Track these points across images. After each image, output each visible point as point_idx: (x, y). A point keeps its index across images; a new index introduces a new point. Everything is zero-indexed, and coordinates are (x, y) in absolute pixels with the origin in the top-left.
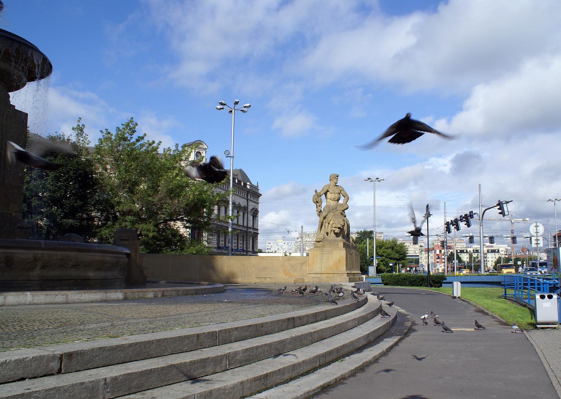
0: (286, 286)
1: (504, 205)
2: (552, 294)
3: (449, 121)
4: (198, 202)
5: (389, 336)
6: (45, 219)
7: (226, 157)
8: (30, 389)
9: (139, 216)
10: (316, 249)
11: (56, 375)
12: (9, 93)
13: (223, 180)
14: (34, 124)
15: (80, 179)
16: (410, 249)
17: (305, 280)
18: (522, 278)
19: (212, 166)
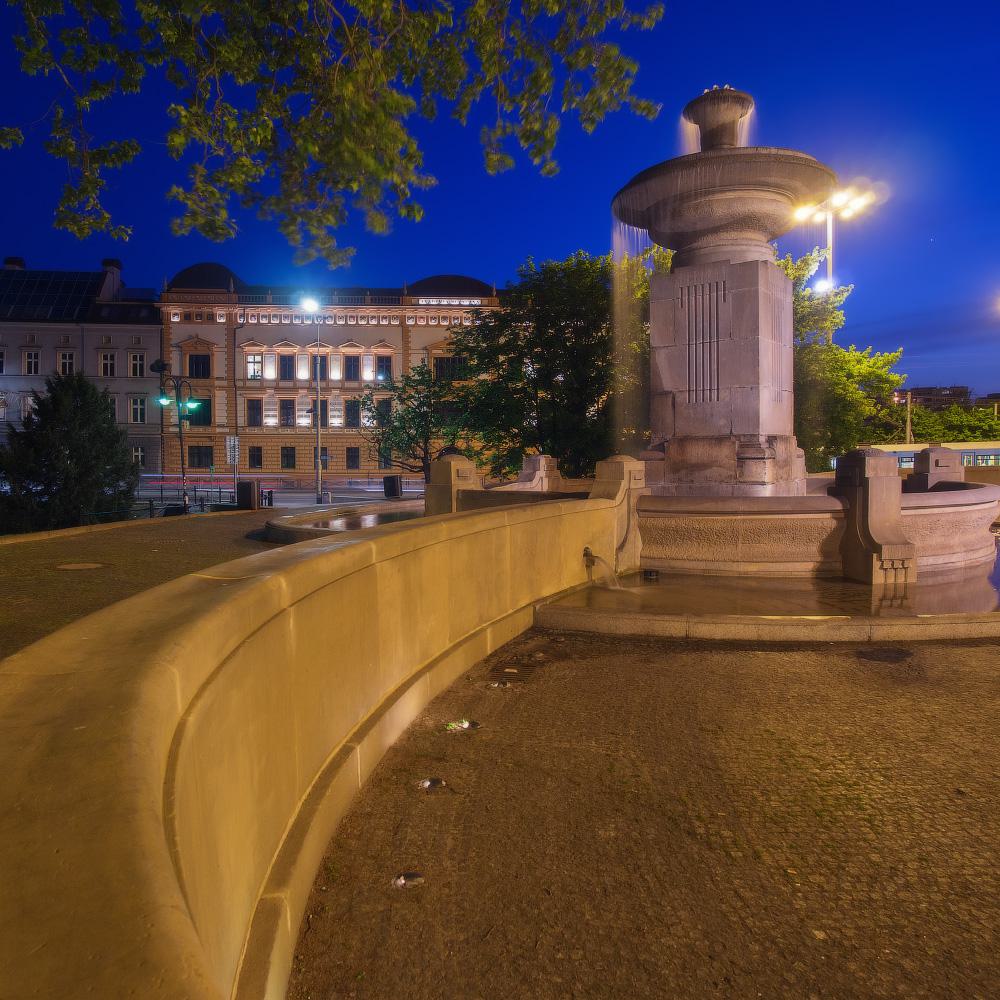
0: (684, 276)
1: (224, 375)
2: (762, 439)
3: (812, 216)
4: (518, 22)
5: (68, 620)
6: (317, 149)
7: (36, 372)
8: (725, 300)
9: (332, 153)
10: (386, 527)
11: (945, 388)
12: (683, 119)
13: (420, 147)
14: (483, 976)
15: (560, 378)
16: (726, 146)
17: (586, 580)
18: (232, 290)
19: (507, 670)
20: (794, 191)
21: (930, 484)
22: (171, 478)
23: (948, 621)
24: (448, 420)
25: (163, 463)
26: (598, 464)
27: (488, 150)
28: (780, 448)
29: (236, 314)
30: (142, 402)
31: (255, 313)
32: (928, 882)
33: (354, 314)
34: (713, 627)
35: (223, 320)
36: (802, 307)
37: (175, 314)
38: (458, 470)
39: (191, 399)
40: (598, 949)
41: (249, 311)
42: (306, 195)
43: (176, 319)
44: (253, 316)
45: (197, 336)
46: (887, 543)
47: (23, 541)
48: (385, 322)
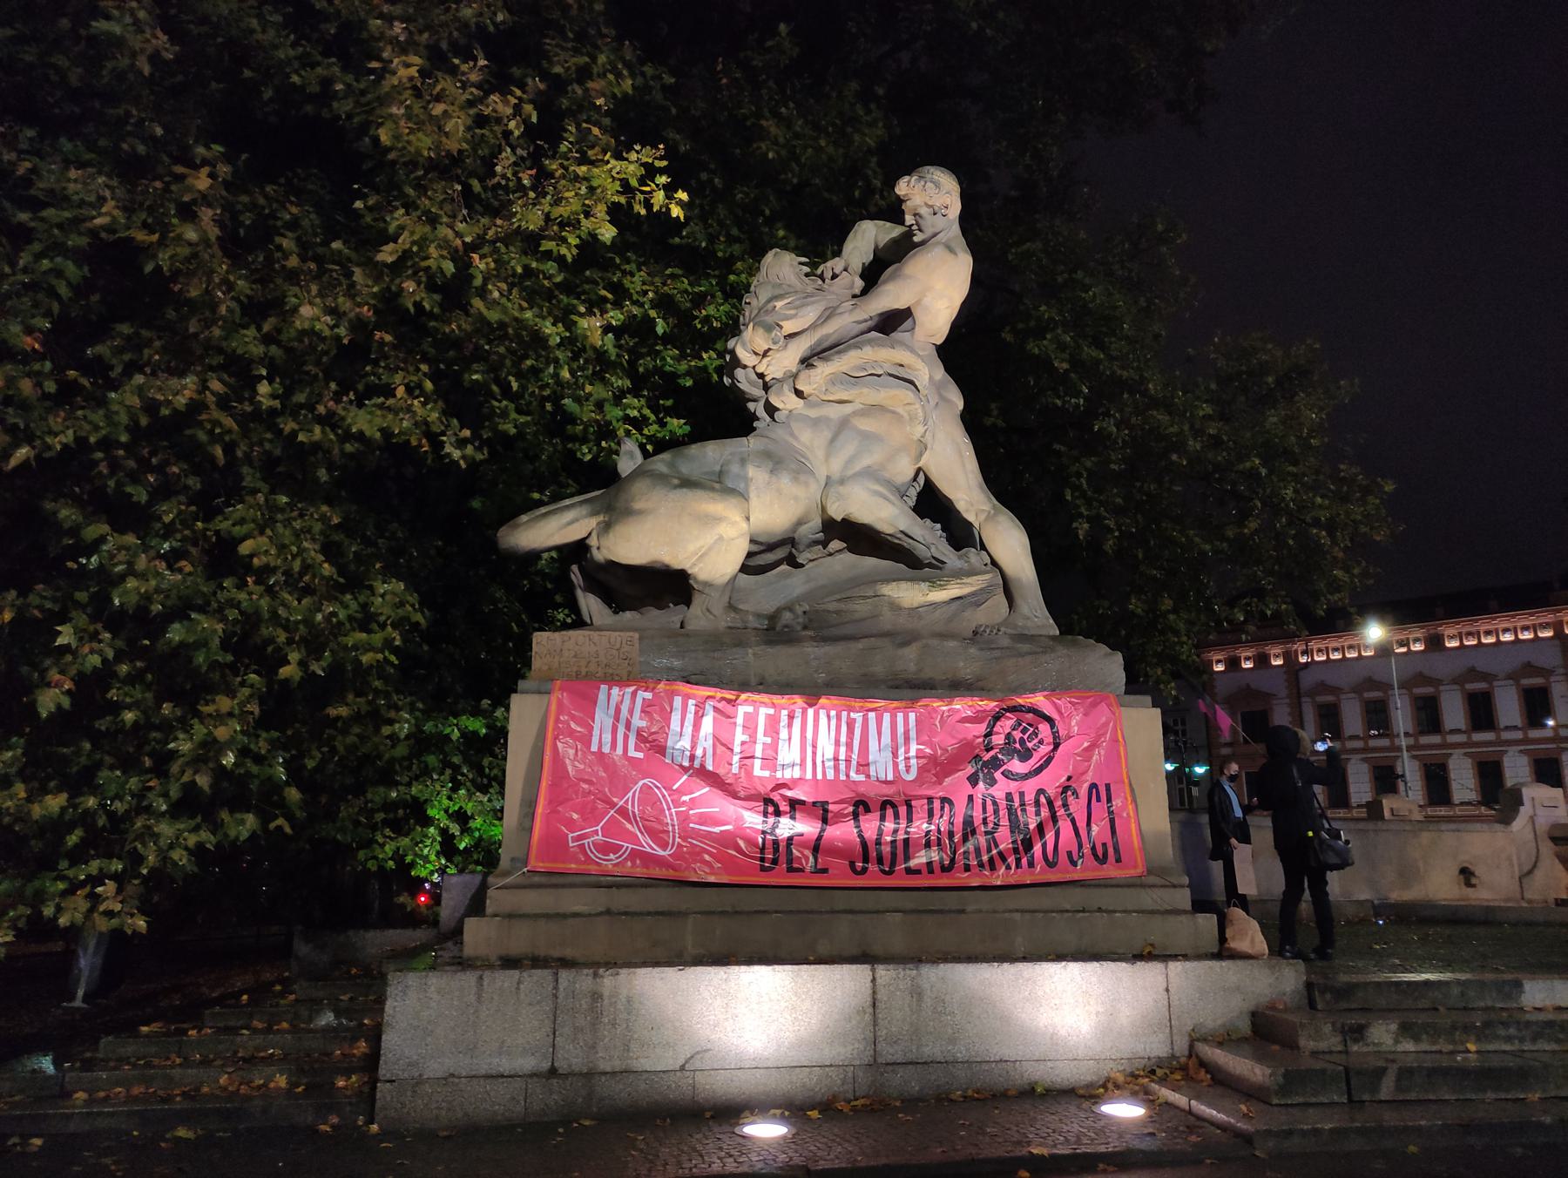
20: (629, 1000)
21: (489, 910)
22: (547, 818)
23: (842, 756)
24: (337, 418)
25: (1004, 912)
26: (839, 519)
27: (288, 335)
28: (982, 517)
29: (1296, 651)
30: (1183, 723)
31: (1322, 646)
32: (518, 336)
33: (1473, 629)
34: (1231, 1057)
35: (1279, 662)
36: (416, 855)
37: (1218, 661)
38: (1392, 810)
39: (1199, 763)
40: (284, 337)
41: (1314, 645)
42: (286, 1055)
43: (1220, 668)
44: (1320, 650)
45: (1248, 685)
46: (1185, 912)
47: (1203, 1107)
48: (1527, 636)
